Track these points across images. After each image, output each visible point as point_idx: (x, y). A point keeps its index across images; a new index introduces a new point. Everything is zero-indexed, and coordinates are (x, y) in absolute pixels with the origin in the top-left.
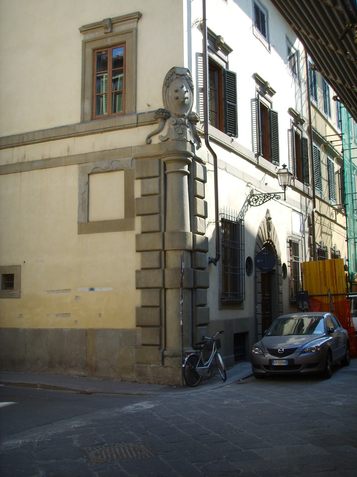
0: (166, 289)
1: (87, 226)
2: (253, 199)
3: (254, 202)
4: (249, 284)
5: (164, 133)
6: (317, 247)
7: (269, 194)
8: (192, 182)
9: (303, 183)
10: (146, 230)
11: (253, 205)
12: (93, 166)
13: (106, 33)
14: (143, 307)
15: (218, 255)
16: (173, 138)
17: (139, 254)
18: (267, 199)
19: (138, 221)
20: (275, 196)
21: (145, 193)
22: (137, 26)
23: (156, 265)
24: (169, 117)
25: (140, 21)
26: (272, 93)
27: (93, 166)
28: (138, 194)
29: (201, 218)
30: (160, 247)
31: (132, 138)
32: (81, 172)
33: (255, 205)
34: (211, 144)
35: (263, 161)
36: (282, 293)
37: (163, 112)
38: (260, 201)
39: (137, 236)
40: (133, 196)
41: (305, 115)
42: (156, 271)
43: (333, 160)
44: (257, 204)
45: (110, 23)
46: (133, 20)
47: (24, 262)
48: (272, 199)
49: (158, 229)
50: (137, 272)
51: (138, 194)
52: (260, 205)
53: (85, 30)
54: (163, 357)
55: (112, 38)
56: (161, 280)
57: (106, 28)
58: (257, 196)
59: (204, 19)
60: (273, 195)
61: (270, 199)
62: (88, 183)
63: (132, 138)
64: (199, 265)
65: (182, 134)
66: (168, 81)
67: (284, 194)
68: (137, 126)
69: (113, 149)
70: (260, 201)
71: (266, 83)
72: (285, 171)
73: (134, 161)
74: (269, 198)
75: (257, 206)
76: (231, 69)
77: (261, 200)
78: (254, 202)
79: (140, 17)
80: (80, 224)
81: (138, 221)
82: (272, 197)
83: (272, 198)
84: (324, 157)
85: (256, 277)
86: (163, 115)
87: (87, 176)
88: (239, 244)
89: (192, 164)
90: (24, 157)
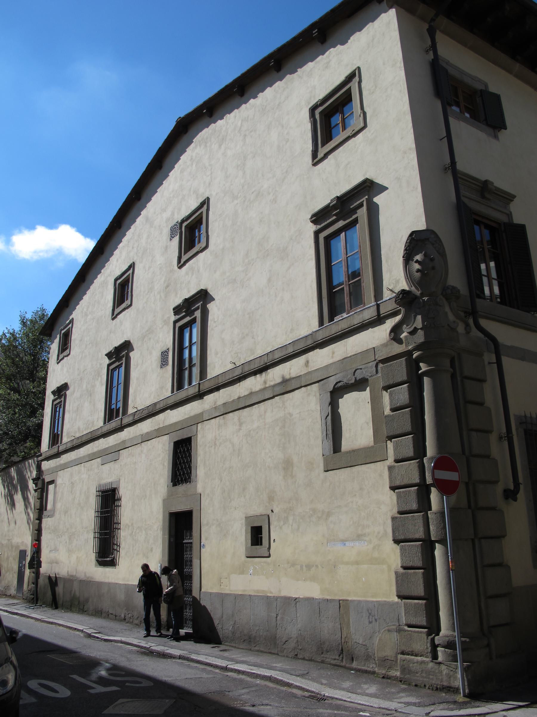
30: (417, 481)
34: (483, 323)
39: (390, 468)
50: (393, 519)
51: (387, 411)
53: (318, 217)
54: (434, 647)
59: (453, 162)
69: (353, 355)
76: (517, 219)
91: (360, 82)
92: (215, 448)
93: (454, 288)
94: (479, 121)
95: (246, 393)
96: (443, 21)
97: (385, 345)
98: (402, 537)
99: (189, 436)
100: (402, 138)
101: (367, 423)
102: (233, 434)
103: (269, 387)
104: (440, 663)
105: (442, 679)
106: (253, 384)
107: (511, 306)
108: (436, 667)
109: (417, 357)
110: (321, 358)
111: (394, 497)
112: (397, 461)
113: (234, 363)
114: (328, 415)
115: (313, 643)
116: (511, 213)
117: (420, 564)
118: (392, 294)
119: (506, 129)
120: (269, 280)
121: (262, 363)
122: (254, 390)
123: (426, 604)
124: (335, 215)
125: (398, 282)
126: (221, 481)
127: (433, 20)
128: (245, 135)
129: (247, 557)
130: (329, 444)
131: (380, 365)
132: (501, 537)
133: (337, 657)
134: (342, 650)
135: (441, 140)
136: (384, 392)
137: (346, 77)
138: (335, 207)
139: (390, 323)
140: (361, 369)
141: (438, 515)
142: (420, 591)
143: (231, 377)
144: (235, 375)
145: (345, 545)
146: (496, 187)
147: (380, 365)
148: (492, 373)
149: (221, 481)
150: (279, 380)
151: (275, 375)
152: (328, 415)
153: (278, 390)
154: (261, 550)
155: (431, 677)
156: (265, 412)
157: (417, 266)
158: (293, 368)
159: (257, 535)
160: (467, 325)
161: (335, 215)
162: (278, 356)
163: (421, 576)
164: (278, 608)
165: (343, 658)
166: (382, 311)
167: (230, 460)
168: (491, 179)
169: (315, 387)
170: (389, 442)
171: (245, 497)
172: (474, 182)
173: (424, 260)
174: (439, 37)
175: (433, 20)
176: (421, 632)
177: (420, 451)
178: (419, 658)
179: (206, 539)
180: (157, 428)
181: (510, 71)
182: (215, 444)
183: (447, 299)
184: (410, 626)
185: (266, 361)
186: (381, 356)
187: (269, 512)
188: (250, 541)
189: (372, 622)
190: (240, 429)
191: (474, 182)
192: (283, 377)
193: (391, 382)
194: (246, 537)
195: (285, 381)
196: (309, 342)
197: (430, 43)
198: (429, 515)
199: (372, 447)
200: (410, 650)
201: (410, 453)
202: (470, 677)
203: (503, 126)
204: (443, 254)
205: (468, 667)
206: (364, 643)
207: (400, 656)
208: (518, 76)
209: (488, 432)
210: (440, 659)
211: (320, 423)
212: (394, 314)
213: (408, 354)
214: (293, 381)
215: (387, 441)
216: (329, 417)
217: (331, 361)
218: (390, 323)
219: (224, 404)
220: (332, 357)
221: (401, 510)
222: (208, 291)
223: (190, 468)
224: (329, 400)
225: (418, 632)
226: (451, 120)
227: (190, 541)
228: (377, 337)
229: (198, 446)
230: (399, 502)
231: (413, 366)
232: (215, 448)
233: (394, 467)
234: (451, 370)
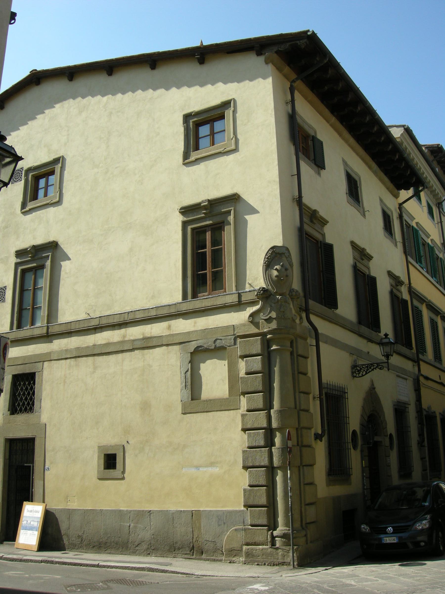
3: (357, 373)
4: (356, 460)
6: (424, 413)
7: (372, 364)
9: (402, 298)
11: (356, 377)
12: (199, 353)
15: (323, 431)
18: (370, 370)
19: (244, 401)
23: (262, 443)
26: (370, 258)
30: (265, 425)
33: (357, 376)
34: (313, 318)
35: (364, 330)
36: (390, 466)
38: (363, 372)
39: (243, 416)
41: (404, 278)
43: (396, 281)
44: (360, 375)
48: (375, 370)
50: (244, 452)
51: (242, 373)
52: (363, 376)
53: (185, 211)
54: (273, 538)
58: (360, 367)
59: (300, 196)
61: (373, 370)
64: (305, 443)
67: (387, 364)
70: (363, 372)
71: (364, 250)
72: (387, 340)
74: (372, 368)
77: (364, 371)
82: (375, 367)
84: (426, 314)
85: (362, 451)
88: (344, 417)
91: (235, 112)
92: (64, 385)
94: (309, 159)
95: (103, 342)
96: (299, 84)
97: (244, 325)
98: (251, 464)
100: (268, 170)
101: (223, 380)
102: (86, 375)
103: (129, 340)
104: (277, 549)
105: (278, 558)
108: (275, 550)
109: (269, 338)
110: (182, 326)
111: (246, 436)
112: (248, 411)
113: (88, 314)
114: (187, 371)
115: (165, 543)
116: (325, 233)
117: (264, 483)
118: (250, 288)
119: (325, 169)
120: (131, 250)
121: (122, 320)
122: (111, 341)
123: (267, 510)
124: (204, 213)
125: (256, 279)
126: (71, 414)
127: (293, 81)
128: (111, 113)
129: (100, 479)
130: (187, 394)
131: (239, 340)
132: (312, 465)
133: (188, 552)
134: (193, 546)
136: (240, 360)
137: (222, 103)
138: (205, 207)
139: (251, 310)
140: (221, 339)
141: (281, 449)
142: (263, 500)
143: (86, 326)
144: (90, 325)
145: (199, 469)
147: (239, 340)
149: (71, 414)
151: (135, 333)
152: (187, 371)
153: (138, 344)
154: (116, 473)
155: (269, 558)
156: (123, 361)
157: (275, 273)
159: (110, 461)
160: (301, 318)
161: (204, 213)
162: (139, 316)
163: (264, 491)
164: (131, 519)
165: (193, 552)
166: (243, 299)
167: (82, 397)
168: (318, 210)
169: (177, 348)
170: (242, 396)
171: (98, 429)
172: (308, 210)
173: (281, 269)
174: (297, 94)
175: (293, 81)
176: (263, 529)
177: (268, 406)
178: (261, 547)
179: (51, 463)
181: (328, 121)
182: (65, 382)
183: (291, 299)
184: (252, 526)
185: (126, 319)
187: (125, 443)
188: (102, 467)
189: (221, 525)
190: (94, 372)
191: (308, 210)
193: (247, 353)
194: (98, 463)
195: (146, 339)
198: (273, 450)
199: (227, 399)
200: (253, 541)
201: (260, 405)
202: (298, 555)
203: (323, 168)
204: (291, 265)
205: (297, 548)
206: (213, 541)
207: (245, 547)
208: (332, 126)
209: (308, 394)
210: (277, 545)
211: (180, 376)
212: (252, 303)
213: (263, 335)
215: (240, 395)
216: (189, 373)
217: (192, 329)
218: (251, 310)
220: (194, 326)
221: (250, 445)
222: (59, 243)
223: (32, 400)
224: (189, 359)
225: (260, 529)
228: (240, 318)
229: (44, 382)
230: (250, 440)
231: (266, 344)
232: (64, 385)
233: (246, 414)
234: (291, 349)
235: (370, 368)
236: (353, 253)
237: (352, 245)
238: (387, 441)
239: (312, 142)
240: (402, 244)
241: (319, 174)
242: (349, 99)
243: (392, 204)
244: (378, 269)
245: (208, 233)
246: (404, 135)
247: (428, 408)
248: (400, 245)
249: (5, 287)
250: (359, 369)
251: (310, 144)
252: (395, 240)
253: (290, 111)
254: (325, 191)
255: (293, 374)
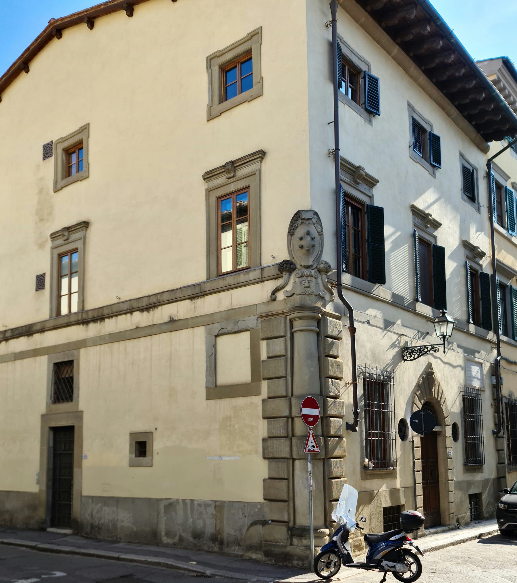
0: (294, 460)
1: (216, 391)
2: (406, 353)
3: (408, 356)
5: (289, 288)
6: (504, 400)
7: (425, 346)
8: (323, 340)
10: (272, 395)
11: (406, 360)
12: (224, 325)
13: (228, 179)
14: (270, 478)
16: (298, 293)
17: (266, 421)
19: (264, 385)
20: (433, 348)
21: (270, 355)
22: (261, 166)
24: (294, 269)
25: (264, 161)
27: (224, 325)
28: (264, 356)
29: (334, 380)
31: (255, 295)
32: (209, 333)
33: (409, 359)
34: (347, 295)
37: (287, 264)
40: (260, 358)
42: (283, 440)
44: (412, 358)
45: (232, 167)
46: (256, 160)
47: (156, 429)
49: (284, 394)
51: (264, 356)
52: (414, 359)
53: (208, 176)
55: (235, 183)
56: (288, 449)
57: (229, 172)
59: (337, 149)
60: (430, 347)
62: (215, 346)
63: (255, 295)
65: (309, 287)
66: (292, 228)
68: (262, 281)
69: (238, 308)
73: (260, 320)
74: (425, 350)
75: (411, 360)
76: (377, 203)
77: (416, 353)
78: (408, 356)
79: (264, 156)
80: (208, 389)
81: (264, 385)
82: (429, 349)
83: (429, 351)
86: (286, 267)
87: (214, 337)
89: (322, 321)
90: (418, 221)
93: (326, 263)
97: (267, 303)
99: (70, 359)
106: (140, 319)
107: (363, 279)
116: (373, 195)
135: (329, 123)
146: (366, 173)
148: (346, 337)
150: (167, 319)
158: (182, 309)
159: (141, 448)
162: (165, 297)
169: (203, 328)
174: (340, 14)
180: (33, 347)
181: (389, 52)
186: (263, 310)
187: (153, 430)
192: (171, 318)
196: (197, 290)
197: (330, 18)
199: (249, 384)
208: (395, 59)
214: (181, 323)
219: (110, 334)
226: (340, 105)
227: (70, 452)
234: (318, 330)
235: (424, 350)
236: (414, 219)
237: (412, 210)
238: (449, 431)
239: (363, 80)
240: (488, 209)
241: (370, 122)
242: (413, 17)
243: (478, 160)
244: (448, 238)
245: (232, 201)
246: (503, 70)
247: (510, 395)
248: (485, 211)
249: (44, 274)
250: (410, 351)
251: (361, 83)
252: (478, 204)
253: (331, 39)
254: (380, 145)
255: (319, 357)
